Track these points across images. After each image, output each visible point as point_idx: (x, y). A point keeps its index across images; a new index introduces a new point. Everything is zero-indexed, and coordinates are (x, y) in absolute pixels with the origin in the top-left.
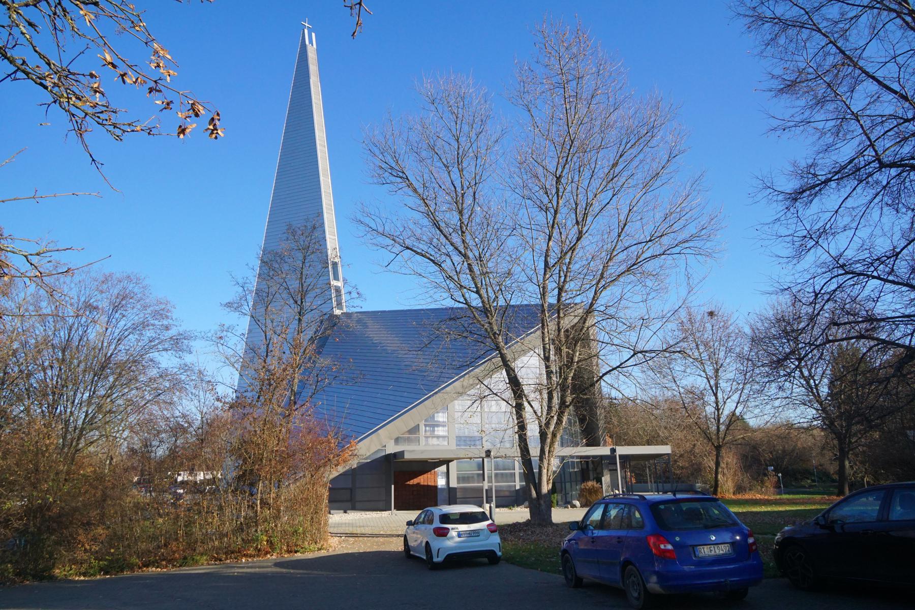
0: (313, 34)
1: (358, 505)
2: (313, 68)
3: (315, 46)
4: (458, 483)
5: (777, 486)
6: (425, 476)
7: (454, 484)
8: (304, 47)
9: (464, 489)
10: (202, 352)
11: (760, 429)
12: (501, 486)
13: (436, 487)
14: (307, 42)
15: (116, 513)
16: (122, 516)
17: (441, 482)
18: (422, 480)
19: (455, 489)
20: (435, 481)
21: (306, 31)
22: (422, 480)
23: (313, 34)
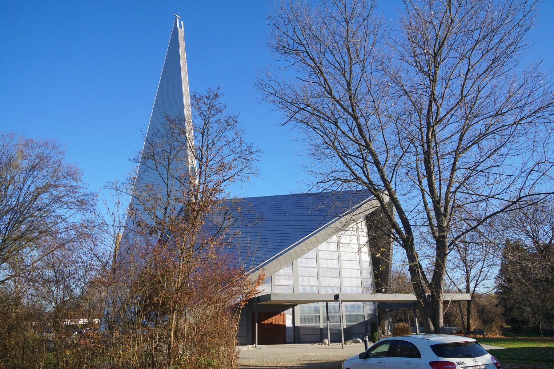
0: (182, 22)
1: (181, 115)
2: (182, 43)
3: (183, 29)
4: (301, 322)
5: (504, 331)
6: (277, 316)
7: (298, 324)
8: (176, 29)
9: (305, 328)
10: (100, 203)
11: (374, 310)
12: (335, 326)
13: (285, 326)
14: (178, 26)
15: (17, 343)
16: (24, 348)
17: (289, 323)
18: (274, 320)
19: (299, 327)
20: (284, 321)
21: (178, 20)
22: (274, 320)
23: (182, 22)
